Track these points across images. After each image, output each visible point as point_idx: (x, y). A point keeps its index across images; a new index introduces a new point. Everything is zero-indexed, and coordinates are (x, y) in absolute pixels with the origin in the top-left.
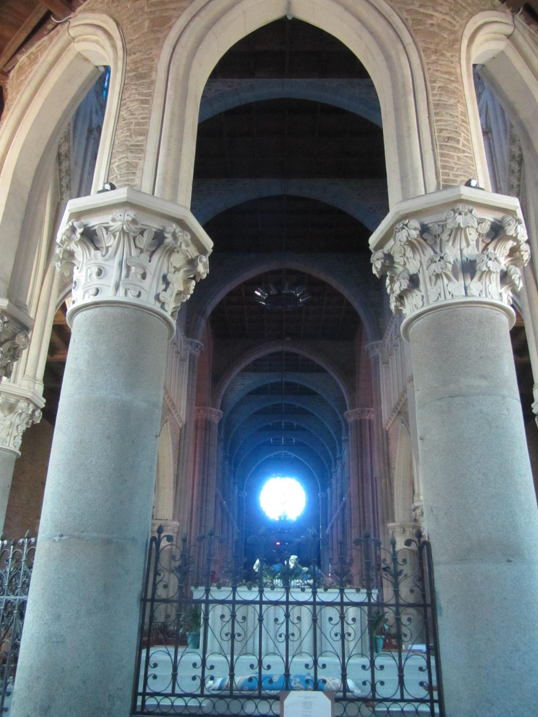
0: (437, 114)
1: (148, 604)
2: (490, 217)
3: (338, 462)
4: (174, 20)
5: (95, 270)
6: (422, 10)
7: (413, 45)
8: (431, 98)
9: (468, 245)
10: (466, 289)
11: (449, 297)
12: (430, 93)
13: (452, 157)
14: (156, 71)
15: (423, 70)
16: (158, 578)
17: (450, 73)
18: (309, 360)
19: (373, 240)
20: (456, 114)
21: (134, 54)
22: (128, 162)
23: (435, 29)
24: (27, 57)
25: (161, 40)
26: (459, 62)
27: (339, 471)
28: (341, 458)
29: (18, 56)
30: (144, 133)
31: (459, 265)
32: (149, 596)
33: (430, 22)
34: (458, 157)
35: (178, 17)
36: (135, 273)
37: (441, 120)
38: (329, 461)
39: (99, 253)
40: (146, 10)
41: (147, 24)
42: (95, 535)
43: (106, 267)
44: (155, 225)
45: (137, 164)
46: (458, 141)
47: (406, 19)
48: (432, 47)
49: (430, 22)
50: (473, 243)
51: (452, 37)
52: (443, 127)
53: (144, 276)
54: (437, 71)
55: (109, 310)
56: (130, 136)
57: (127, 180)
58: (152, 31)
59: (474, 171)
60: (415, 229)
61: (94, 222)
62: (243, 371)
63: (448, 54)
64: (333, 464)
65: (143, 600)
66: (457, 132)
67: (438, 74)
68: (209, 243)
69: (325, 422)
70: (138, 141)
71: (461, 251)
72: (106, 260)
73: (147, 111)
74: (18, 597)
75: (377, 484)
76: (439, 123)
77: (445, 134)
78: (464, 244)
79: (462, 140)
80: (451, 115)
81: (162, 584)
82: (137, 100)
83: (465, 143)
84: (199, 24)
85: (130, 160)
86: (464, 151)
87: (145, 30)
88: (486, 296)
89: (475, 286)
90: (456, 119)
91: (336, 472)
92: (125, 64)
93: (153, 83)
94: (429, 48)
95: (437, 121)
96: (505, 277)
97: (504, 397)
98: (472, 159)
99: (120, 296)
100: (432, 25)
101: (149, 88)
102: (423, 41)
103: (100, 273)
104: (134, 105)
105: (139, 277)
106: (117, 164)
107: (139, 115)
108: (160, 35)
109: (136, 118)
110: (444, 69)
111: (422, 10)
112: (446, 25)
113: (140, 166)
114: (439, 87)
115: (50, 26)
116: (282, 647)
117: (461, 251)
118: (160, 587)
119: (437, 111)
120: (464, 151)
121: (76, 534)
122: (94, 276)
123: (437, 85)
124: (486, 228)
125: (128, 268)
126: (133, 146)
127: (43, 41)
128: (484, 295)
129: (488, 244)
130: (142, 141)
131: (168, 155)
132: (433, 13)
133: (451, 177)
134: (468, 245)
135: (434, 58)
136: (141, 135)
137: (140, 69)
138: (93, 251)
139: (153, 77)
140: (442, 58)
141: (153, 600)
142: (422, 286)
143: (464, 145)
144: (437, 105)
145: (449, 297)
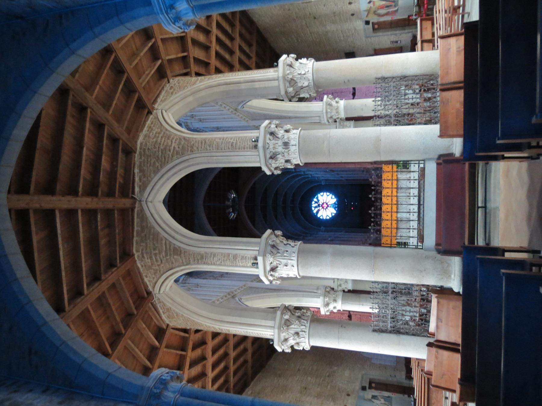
0: (221, 149)
1: (392, 245)
2: (268, 136)
3: (306, 173)
4: (176, 246)
5: (285, 267)
6: (172, 151)
7: (189, 156)
8: (215, 151)
9: (277, 143)
10: (293, 145)
11: (296, 151)
12: (212, 151)
13: (240, 145)
14: (201, 251)
15: (202, 153)
16: (385, 243)
17: (202, 143)
18: (210, 185)
19: (268, 173)
20: (221, 142)
21: (190, 261)
22: (241, 260)
23: (181, 147)
24: (164, 314)
25: (185, 250)
26: (195, 138)
27: (311, 173)
28: (304, 172)
29: (163, 318)
30: (229, 255)
31: (284, 147)
32: (390, 245)
33: (177, 148)
34: (239, 143)
35: (174, 244)
36: (287, 254)
37: (224, 148)
38: (304, 178)
39: (279, 266)
40: (168, 257)
41: (175, 257)
42: (372, 261)
43: (284, 263)
44: (269, 248)
45: (242, 256)
46: (233, 142)
47: (177, 157)
48: (190, 149)
49: (177, 148)
50: (276, 142)
51: (183, 140)
52: (227, 147)
53: (287, 251)
54: (201, 147)
55: (299, 262)
56: (229, 259)
57: (249, 259)
58: (180, 254)
59: (244, 138)
60: (272, 161)
61: (268, 268)
62: (254, 225)
63: (192, 143)
64: (299, 173)
65: (391, 247)
66: (229, 143)
67: (203, 147)
68: (269, 231)
69: (283, 181)
70: (232, 257)
71: (279, 146)
72: (282, 264)
73: (219, 254)
74: (390, 289)
75: (218, 87)
76: (225, 148)
77: (230, 147)
78: (277, 145)
79: (232, 141)
80: (221, 144)
81: (386, 242)
82: (213, 258)
83: (233, 139)
84: (177, 236)
85: (240, 259)
86: (236, 140)
87: (179, 257)
88: (296, 139)
89: (292, 142)
90: (223, 142)
91: (311, 175)
92: (194, 264)
93: (206, 253)
94: (191, 150)
95: (225, 149)
96: (287, 131)
97: (330, 137)
98: (239, 138)
99: (295, 258)
100: (178, 147)
101: (208, 254)
102: (187, 151)
103: (286, 266)
104: (215, 259)
105: (287, 252)
106: (241, 264)
107: (220, 257)
108: (183, 251)
109: (222, 258)
110: (200, 145)
111: (172, 151)
112: (177, 142)
113: (243, 255)
114: (209, 147)
115: (155, 303)
116: (404, 206)
117: (279, 146)
118: (387, 242)
119: (220, 149)
120: (236, 140)
121: (372, 266)
122: (287, 267)
123: (208, 148)
124: (271, 137)
125: (285, 256)
126: (234, 258)
127: (160, 306)
128: (296, 140)
129: (276, 136)
130: (232, 255)
131: (238, 246)
132: (173, 147)
133: (248, 146)
134: (277, 143)
135: (195, 148)
136: (229, 255)
137: (198, 258)
138: (278, 268)
139: (203, 253)
140: (195, 145)
141: (391, 244)
142: (289, 159)
143: (234, 140)
144: (218, 149)
145: (296, 151)
